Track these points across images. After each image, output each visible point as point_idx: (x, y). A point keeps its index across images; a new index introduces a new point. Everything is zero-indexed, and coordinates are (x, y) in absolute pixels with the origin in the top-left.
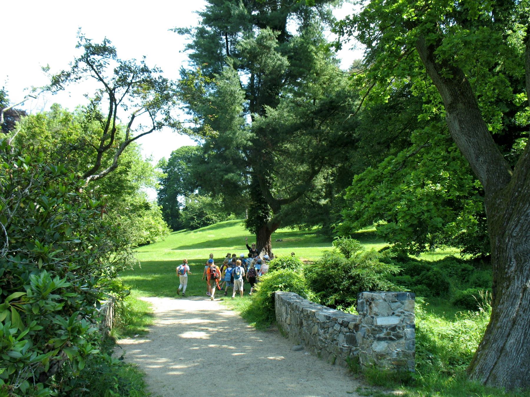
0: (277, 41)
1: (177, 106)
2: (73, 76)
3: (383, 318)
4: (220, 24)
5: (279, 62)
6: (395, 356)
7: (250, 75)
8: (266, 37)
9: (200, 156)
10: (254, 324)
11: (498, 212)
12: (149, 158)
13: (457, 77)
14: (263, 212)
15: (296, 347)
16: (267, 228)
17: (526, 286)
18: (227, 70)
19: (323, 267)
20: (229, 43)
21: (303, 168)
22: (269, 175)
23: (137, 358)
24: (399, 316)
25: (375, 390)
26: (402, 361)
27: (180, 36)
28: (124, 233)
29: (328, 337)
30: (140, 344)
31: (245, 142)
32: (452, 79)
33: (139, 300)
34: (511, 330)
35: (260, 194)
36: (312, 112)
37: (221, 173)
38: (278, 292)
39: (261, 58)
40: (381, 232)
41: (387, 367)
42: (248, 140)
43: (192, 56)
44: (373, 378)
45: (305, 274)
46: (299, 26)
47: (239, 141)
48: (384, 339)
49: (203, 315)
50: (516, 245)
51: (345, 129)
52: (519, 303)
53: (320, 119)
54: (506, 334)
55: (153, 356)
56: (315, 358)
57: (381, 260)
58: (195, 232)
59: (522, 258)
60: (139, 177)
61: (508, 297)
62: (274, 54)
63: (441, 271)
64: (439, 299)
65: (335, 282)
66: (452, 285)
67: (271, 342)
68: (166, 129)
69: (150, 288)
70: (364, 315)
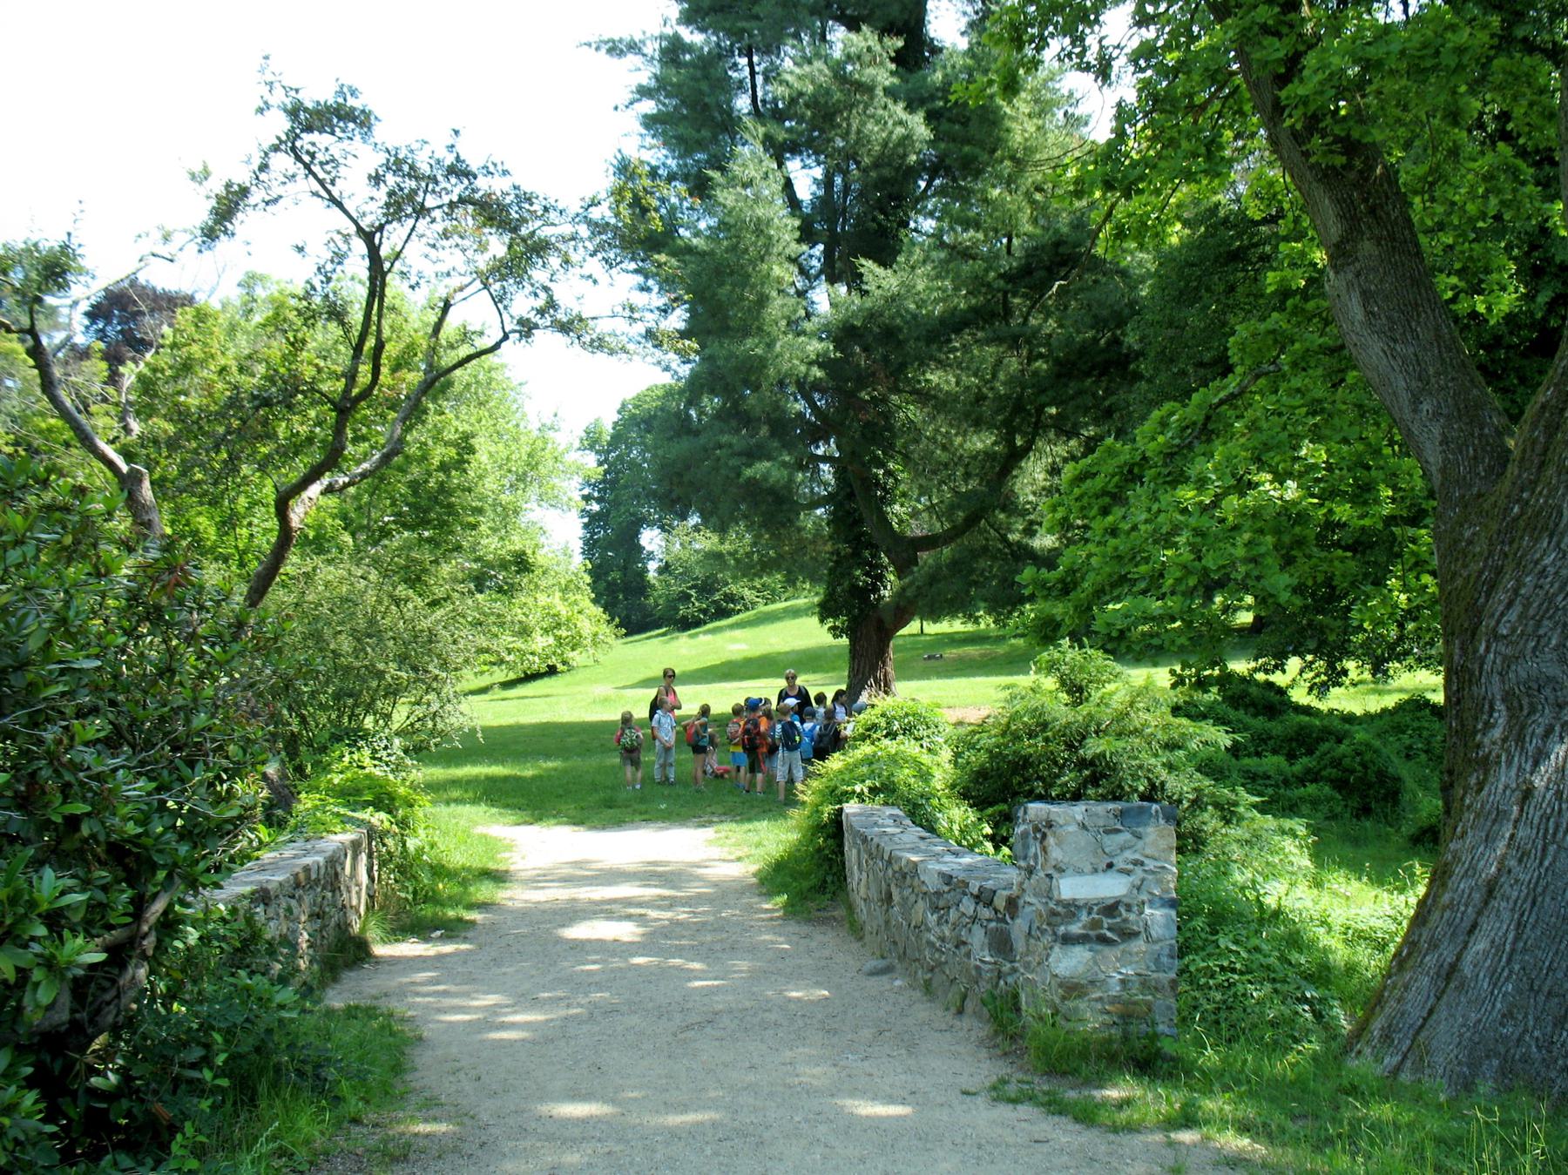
0: (893, 67)
1: (577, 270)
2: (256, 196)
3: (1079, 880)
4: (727, 25)
5: (900, 131)
6: (1115, 989)
7: (818, 172)
8: (859, 58)
9: (678, 414)
10: (782, 899)
11: (1465, 566)
12: (549, 423)
13: (1358, 163)
14: (867, 574)
15: (873, 963)
16: (880, 621)
17: (1531, 783)
18: (749, 156)
19: (1003, 734)
20: (759, 79)
21: (981, 442)
22: (882, 465)
23: (418, 994)
24: (1128, 873)
25: (1045, 1088)
26: (1135, 1003)
27: (614, 61)
28: (430, 642)
29: (947, 933)
30: (440, 957)
31: (803, 368)
32: (1343, 167)
33: (458, 832)
34: (1479, 913)
35: (859, 522)
36: (1001, 276)
37: (734, 462)
38: (851, 807)
39: (848, 119)
40: (1108, 624)
41: (1091, 1020)
42: (811, 364)
43: (650, 122)
44: (1045, 1051)
45: (957, 755)
46: (965, 20)
47: (785, 367)
48: (1081, 940)
49: (650, 875)
50: (1508, 661)
51: (1099, 323)
52: (1507, 835)
53: (1025, 296)
54: (1466, 925)
55: (466, 988)
56: (918, 994)
57: (1176, 710)
58: (691, 636)
59: (1525, 702)
60: (522, 478)
61: (1478, 816)
62: (885, 107)
63: (1377, 743)
64: (1368, 824)
65: (1039, 778)
66: (1410, 783)
67: (810, 951)
68: (546, 339)
69: (523, 801)
70: (1030, 871)
